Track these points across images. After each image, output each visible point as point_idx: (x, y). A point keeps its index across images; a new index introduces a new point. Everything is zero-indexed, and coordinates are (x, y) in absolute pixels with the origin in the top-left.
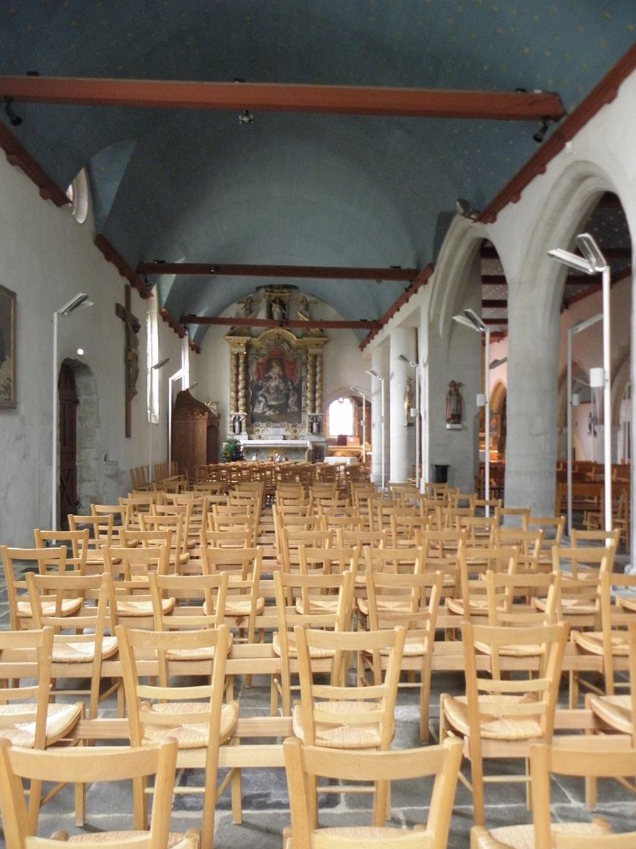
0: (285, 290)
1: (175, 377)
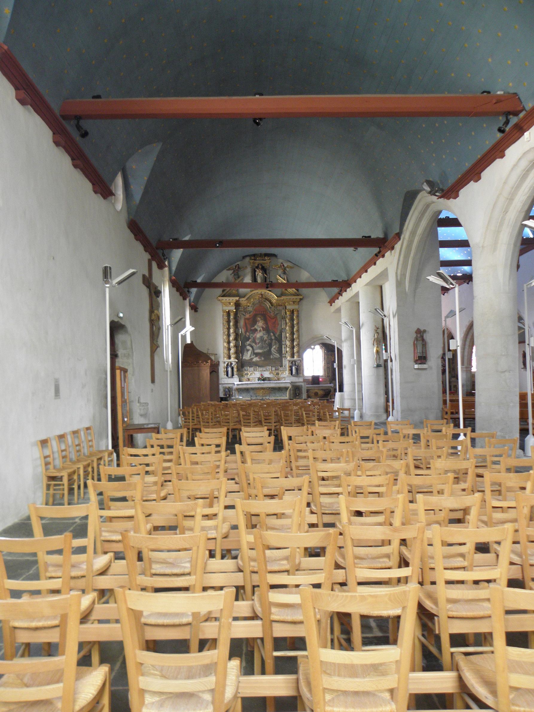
0: (266, 258)
1: (183, 332)
